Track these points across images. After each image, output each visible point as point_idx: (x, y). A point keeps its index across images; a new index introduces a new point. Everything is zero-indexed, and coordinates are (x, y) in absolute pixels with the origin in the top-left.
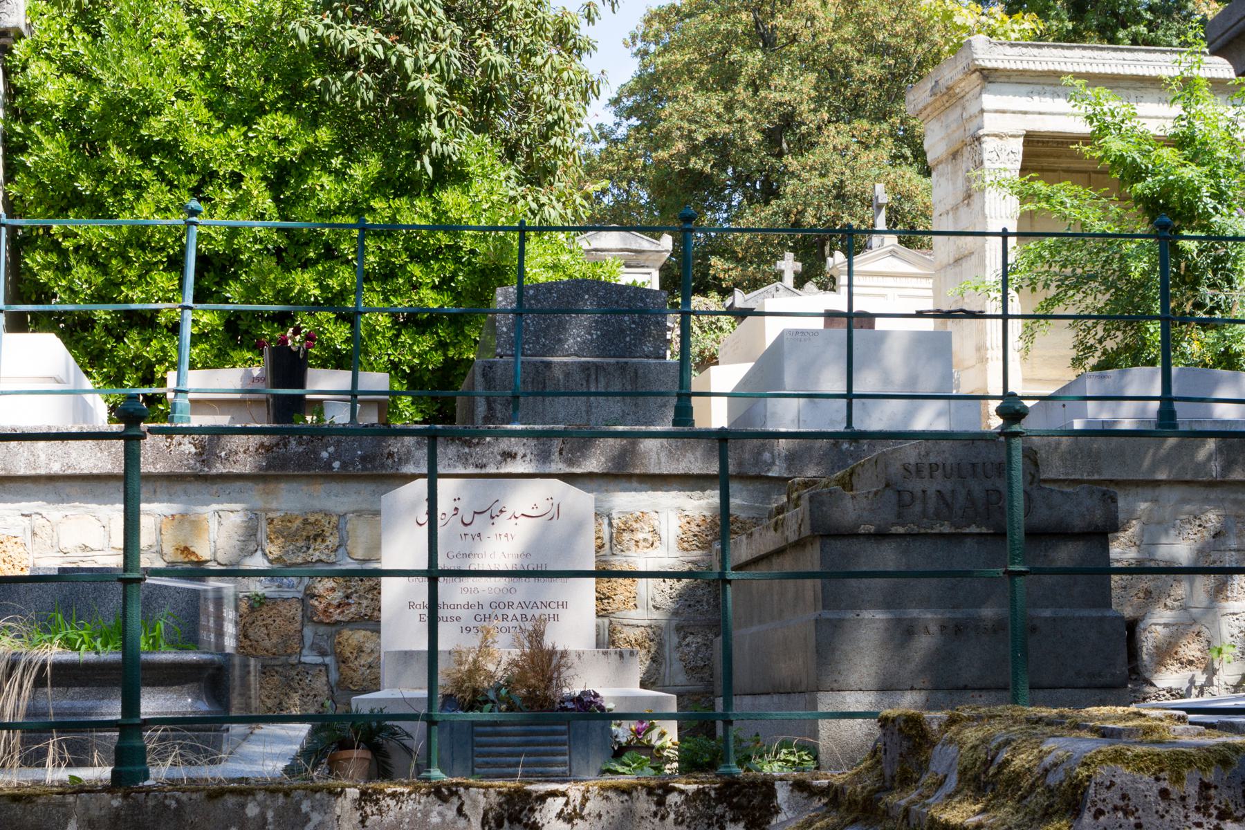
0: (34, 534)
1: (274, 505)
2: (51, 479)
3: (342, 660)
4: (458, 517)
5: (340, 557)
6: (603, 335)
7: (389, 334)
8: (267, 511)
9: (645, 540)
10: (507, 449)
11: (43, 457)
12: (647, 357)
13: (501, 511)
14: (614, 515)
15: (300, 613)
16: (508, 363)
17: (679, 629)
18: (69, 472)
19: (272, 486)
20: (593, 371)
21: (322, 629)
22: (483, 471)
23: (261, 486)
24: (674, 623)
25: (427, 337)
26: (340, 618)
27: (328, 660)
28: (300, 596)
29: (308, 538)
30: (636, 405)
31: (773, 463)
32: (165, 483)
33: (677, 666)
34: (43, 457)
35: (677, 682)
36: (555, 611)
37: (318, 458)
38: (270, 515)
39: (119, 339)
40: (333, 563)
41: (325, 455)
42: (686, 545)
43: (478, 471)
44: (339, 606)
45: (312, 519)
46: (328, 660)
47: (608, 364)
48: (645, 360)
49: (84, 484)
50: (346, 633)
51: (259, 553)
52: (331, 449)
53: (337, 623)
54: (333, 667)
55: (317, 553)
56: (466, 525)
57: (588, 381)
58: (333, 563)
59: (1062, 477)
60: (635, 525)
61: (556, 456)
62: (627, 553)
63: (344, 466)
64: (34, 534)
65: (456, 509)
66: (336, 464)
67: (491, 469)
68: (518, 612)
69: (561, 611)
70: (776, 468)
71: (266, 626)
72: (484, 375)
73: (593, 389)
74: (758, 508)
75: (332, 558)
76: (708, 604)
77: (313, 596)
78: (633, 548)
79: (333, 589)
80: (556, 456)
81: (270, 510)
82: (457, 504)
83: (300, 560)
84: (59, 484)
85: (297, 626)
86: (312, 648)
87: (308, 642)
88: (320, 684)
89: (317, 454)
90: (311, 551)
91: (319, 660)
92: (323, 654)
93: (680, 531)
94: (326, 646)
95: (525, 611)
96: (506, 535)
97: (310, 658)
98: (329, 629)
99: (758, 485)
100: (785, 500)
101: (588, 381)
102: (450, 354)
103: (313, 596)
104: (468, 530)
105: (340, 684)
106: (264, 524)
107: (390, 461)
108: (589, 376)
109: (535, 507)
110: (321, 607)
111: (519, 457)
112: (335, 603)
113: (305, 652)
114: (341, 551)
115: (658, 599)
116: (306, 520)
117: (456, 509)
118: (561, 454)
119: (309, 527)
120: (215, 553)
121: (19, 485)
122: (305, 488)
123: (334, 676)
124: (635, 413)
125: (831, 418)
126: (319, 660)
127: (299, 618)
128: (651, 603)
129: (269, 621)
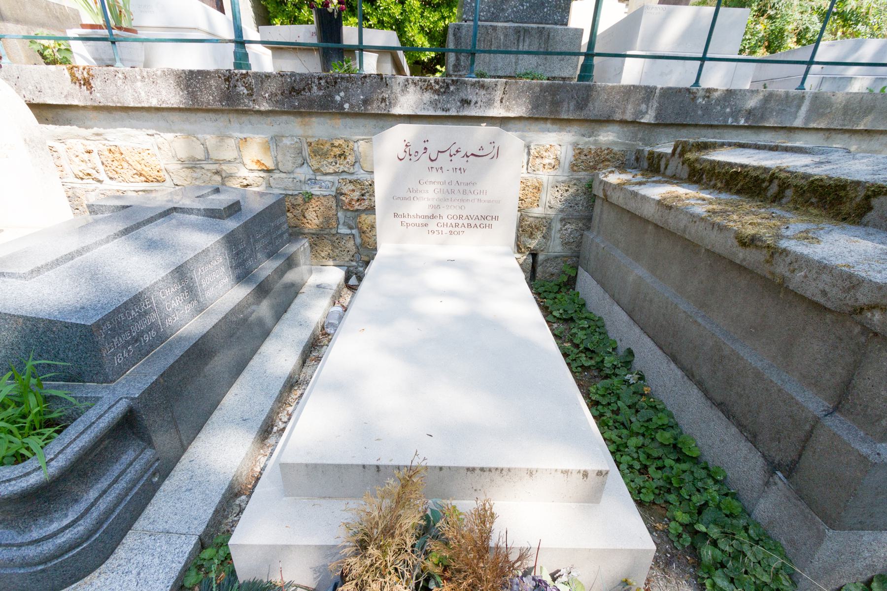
0: (159, 148)
1: (310, 133)
2: (158, 110)
3: (362, 232)
4: (427, 155)
5: (356, 169)
6: (531, 6)
7: (419, 11)
8: (306, 137)
9: (550, 164)
10: (465, 97)
11: (143, 94)
12: (556, 24)
13: (457, 151)
14: (532, 147)
15: (334, 205)
16: (469, 26)
17: (562, 220)
18: (164, 106)
19: (307, 119)
20: (522, 33)
21: (349, 214)
22: (447, 114)
23: (299, 119)
24: (560, 217)
25: (436, 13)
26: (359, 208)
27: (354, 231)
28: (334, 194)
29: (335, 156)
30: (546, 59)
31: (647, 112)
32: (235, 115)
33: (558, 241)
34: (143, 94)
35: (556, 250)
36: (490, 222)
37: (333, 101)
38: (309, 140)
39: (300, 9)
40: (353, 174)
41: (338, 98)
42: (575, 168)
43: (444, 113)
44: (358, 200)
45: (336, 144)
46: (354, 231)
47: (532, 28)
48: (555, 26)
49: (181, 114)
50: (364, 216)
51: (305, 165)
52: (342, 94)
53: (357, 210)
54: (357, 235)
55: (342, 167)
56: (432, 160)
57: (518, 41)
58: (353, 174)
59: (839, 127)
60: (545, 154)
61: (497, 104)
62: (537, 172)
63: (351, 106)
64: (159, 148)
65: (426, 149)
66: (346, 106)
67: (453, 112)
68: (466, 222)
69: (494, 222)
70: (647, 116)
71: (315, 211)
72: (455, 35)
73: (521, 48)
74: (627, 144)
75: (352, 170)
76: (583, 206)
77: (342, 194)
78: (541, 169)
79: (353, 191)
80: (497, 104)
81: (308, 137)
82: (426, 145)
83: (331, 171)
84: (165, 114)
85: (334, 212)
86: (344, 224)
87: (341, 221)
88: (350, 245)
89: (332, 97)
90: (338, 165)
91: (348, 231)
92: (351, 228)
93: (573, 159)
94: (352, 224)
95: (470, 221)
96: (460, 169)
97: (343, 230)
98: (354, 214)
99: (631, 128)
100: (669, 150)
101: (518, 41)
102: (447, 22)
103: (342, 194)
104: (433, 164)
105: (361, 245)
106: (306, 146)
107: (383, 104)
108: (519, 37)
109: (482, 148)
110: (347, 201)
111: (472, 104)
112: (356, 198)
113: (340, 227)
114: (357, 165)
115: (552, 202)
116: (332, 144)
117: (426, 149)
118: (501, 102)
119: (335, 149)
120: (277, 165)
121: (138, 113)
122: (328, 121)
123: (358, 241)
124: (544, 64)
125: (679, 76)
126: (348, 231)
127: (334, 207)
128: (548, 204)
129: (317, 208)
